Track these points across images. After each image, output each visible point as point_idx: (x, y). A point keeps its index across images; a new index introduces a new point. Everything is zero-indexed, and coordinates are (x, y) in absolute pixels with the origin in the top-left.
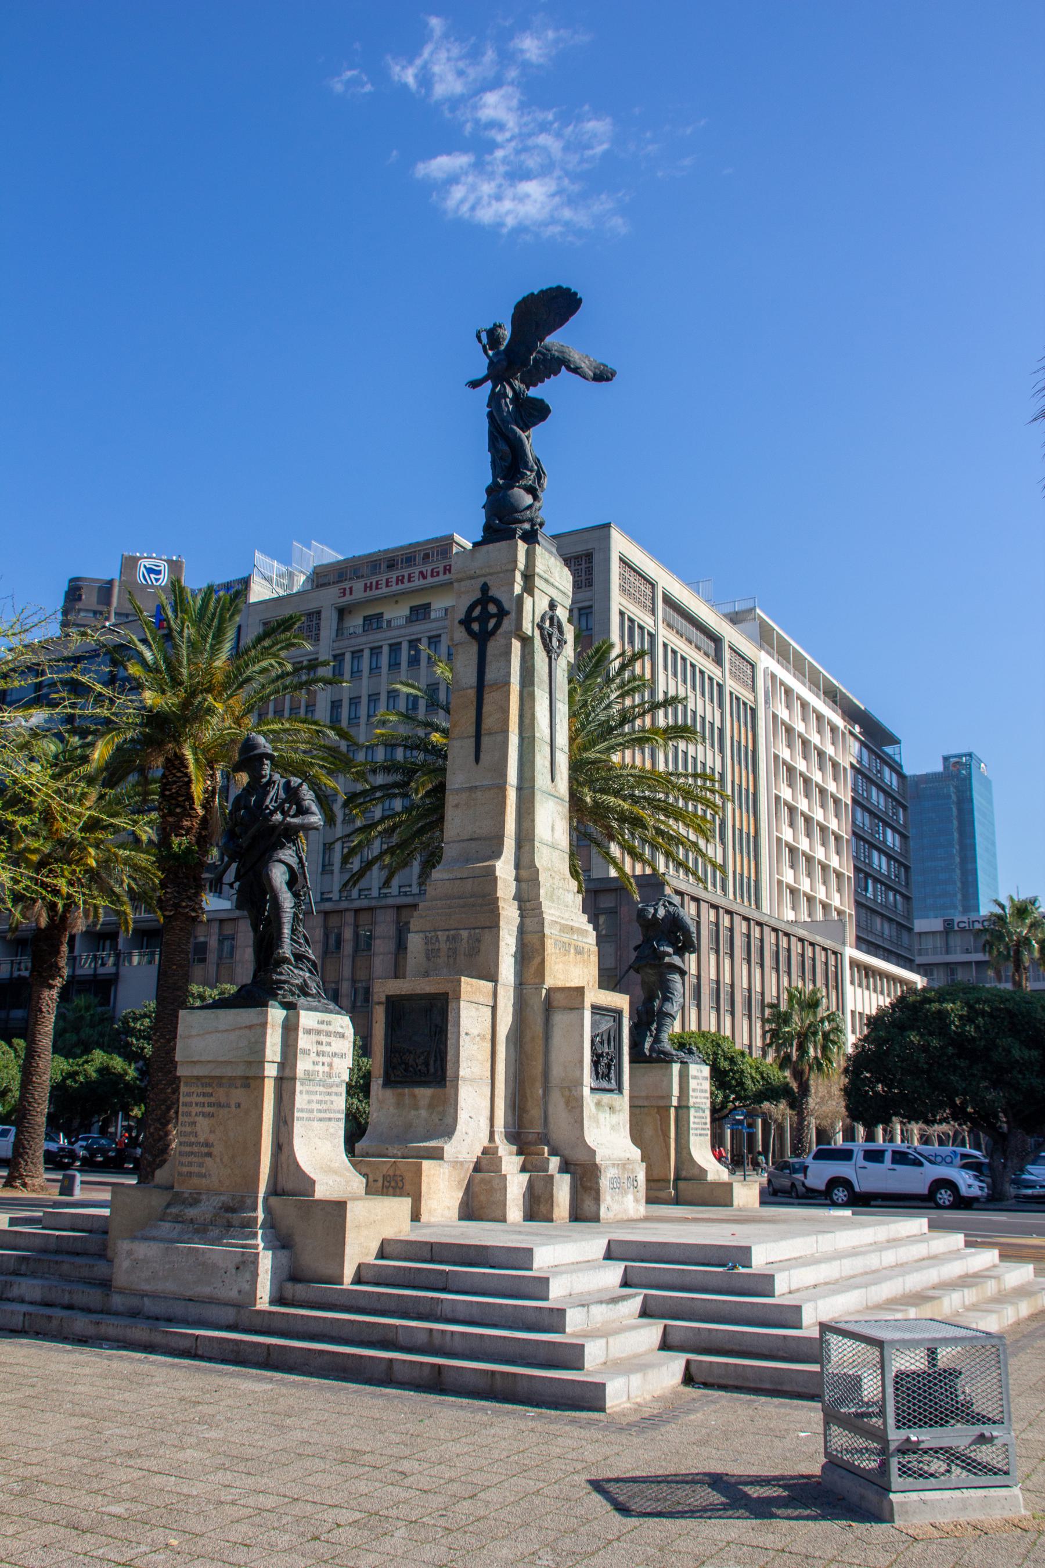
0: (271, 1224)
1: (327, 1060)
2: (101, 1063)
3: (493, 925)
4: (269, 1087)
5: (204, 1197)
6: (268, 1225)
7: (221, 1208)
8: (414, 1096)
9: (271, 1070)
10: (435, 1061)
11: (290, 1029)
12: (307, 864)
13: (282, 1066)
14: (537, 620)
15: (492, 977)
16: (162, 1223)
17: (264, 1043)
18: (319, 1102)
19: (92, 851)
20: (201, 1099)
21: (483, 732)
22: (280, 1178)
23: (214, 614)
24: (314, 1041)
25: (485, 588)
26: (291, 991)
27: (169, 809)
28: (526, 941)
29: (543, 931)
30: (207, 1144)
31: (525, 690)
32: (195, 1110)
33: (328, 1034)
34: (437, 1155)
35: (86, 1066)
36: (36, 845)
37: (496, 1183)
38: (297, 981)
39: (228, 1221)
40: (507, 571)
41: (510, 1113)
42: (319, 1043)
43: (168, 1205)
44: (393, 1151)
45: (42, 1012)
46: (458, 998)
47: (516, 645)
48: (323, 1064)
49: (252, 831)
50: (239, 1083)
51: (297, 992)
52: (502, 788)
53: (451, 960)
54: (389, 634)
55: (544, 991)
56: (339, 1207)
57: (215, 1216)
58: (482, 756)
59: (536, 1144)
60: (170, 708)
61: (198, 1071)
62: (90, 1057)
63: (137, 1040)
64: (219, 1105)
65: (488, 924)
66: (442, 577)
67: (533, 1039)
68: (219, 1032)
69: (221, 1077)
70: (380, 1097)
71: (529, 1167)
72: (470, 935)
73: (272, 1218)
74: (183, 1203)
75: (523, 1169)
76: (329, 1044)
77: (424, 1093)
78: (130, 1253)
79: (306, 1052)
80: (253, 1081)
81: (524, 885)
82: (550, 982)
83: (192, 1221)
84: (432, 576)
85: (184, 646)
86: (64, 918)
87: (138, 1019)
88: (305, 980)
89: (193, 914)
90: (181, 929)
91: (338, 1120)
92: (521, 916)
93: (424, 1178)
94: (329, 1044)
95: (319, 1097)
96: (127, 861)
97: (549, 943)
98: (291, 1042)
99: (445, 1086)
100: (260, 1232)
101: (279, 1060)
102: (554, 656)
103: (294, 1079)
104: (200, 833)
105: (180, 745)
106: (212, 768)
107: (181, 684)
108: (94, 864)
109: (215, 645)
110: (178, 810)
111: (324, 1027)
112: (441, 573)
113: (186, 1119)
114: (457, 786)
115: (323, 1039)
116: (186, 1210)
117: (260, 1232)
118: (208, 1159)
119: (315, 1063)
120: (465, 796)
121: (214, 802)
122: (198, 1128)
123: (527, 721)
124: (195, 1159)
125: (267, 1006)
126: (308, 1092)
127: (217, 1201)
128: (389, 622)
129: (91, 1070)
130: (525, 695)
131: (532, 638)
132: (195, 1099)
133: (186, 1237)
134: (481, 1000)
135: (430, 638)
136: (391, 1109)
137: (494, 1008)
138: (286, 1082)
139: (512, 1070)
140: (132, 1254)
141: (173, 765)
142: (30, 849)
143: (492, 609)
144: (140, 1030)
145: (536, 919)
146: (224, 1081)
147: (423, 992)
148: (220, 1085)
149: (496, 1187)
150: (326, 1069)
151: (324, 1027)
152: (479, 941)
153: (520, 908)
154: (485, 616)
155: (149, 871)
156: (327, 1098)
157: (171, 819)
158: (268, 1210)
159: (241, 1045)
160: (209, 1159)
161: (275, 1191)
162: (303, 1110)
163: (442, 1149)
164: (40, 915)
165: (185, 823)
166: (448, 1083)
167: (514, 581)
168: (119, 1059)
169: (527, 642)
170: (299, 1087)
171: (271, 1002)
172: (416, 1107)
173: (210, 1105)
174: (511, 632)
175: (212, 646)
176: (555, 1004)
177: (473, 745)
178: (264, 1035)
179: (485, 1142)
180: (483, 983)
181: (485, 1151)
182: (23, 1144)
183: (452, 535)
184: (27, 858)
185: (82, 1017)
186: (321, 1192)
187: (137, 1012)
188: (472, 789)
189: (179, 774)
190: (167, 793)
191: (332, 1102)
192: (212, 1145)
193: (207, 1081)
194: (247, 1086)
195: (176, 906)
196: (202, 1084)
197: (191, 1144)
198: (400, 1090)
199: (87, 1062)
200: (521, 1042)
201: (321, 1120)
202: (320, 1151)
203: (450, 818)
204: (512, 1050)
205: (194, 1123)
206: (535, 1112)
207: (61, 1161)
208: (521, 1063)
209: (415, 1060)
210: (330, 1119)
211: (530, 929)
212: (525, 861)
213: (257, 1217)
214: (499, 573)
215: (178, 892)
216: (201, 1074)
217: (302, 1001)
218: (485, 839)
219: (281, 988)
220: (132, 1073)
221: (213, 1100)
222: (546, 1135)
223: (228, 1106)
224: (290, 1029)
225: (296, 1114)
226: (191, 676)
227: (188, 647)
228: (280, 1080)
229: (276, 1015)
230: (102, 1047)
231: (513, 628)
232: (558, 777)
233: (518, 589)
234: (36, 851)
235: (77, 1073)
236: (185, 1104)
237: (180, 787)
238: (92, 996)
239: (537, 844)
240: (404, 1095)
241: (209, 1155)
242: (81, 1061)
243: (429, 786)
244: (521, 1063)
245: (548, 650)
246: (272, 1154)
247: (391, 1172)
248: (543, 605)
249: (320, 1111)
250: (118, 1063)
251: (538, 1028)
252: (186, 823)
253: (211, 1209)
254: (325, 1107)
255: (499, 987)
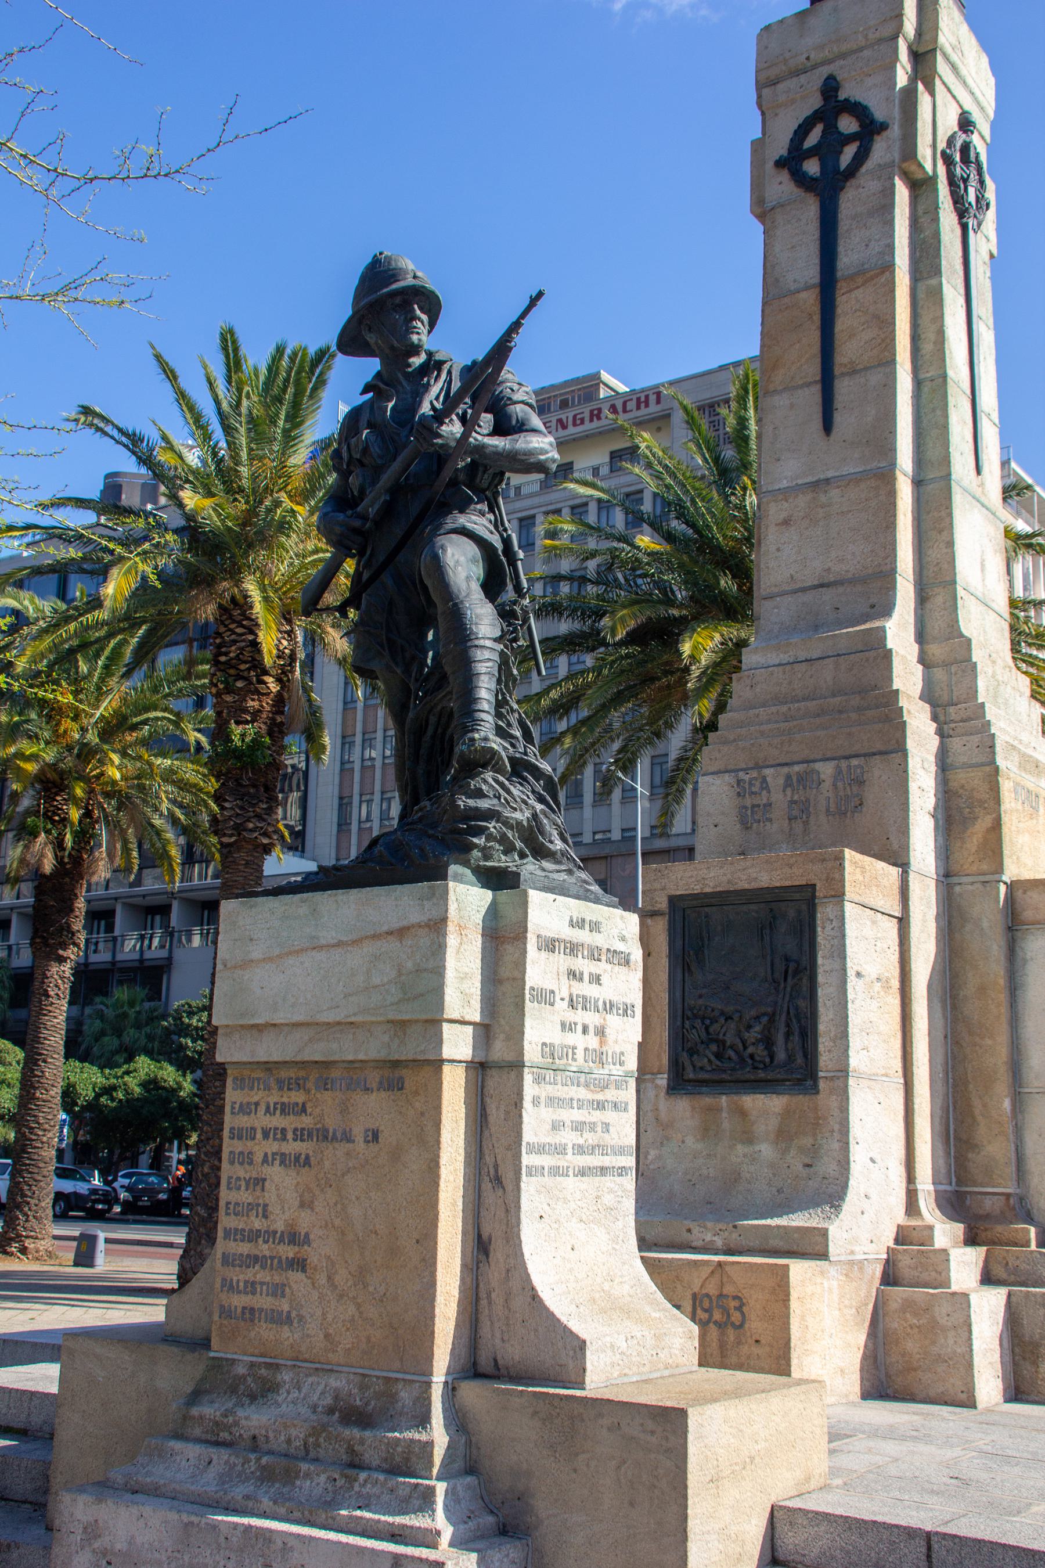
0: (468, 1462)
1: (592, 1019)
2: (147, 1074)
3: (895, 748)
4: (454, 1086)
5: (286, 1376)
6: (459, 1464)
7: (331, 1411)
8: (743, 1113)
9: (458, 1044)
10: (788, 1035)
11: (503, 938)
12: (521, 555)
13: (484, 1032)
14: (941, 145)
15: (897, 855)
16: (177, 1445)
17: (439, 971)
18: (579, 1127)
19: (116, 758)
20: (277, 1121)
21: (837, 371)
22: (485, 1331)
23: (287, 380)
24: (563, 969)
25: (830, 88)
26: (503, 839)
27: (226, 682)
28: (953, 785)
29: (993, 762)
30: (293, 1238)
31: (921, 287)
32: (261, 1148)
33: (595, 954)
34: (813, 1247)
35: (126, 1078)
36: (35, 749)
37: (941, 1312)
38: (518, 815)
39: (351, 1451)
40: (880, 41)
41: (940, 1146)
42: (574, 975)
43: (195, 1396)
44: (702, 1234)
45: (48, 996)
46: (839, 896)
47: (902, 193)
48: (585, 1030)
49: (386, 479)
50: (374, 1077)
51: (519, 844)
52: (887, 477)
53: (798, 827)
54: (518, 505)
55: (1003, 888)
56: (669, 1423)
57: (316, 1431)
58: (838, 418)
59: (1003, 1218)
60: (223, 521)
61: (269, 1049)
62: (132, 1066)
63: (194, 1041)
64: (324, 1135)
65: (879, 746)
66: (588, 426)
67: (982, 989)
68: (319, 948)
69: (327, 1065)
70: (663, 1115)
71: (999, 1272)
72: (839, 771)
73: (469, 1443)
74: (233, 1390)
75: (988, 1279)
76: (596, 979)
77: (766, 1107)
78: (92, 1532)
79: (546, 997)
80: (409, 1074)
81: (939, 674)
82: (1012, 871)
83: (255, 1443)
84: (575, 425)
85: (243, 430)
86: (77, 860)
87: (194, 1013)
88: (535, 816)
89: (265, 841)
90: (247, 863)
91: (622, 1171)
92: (940, 732)
93: (794, 1304)
94: (596, 979)
95: (577, 1115)
96: (169, 776)
97: (1006, 787)
98: (505, 972)
99: (815, 1090)
100: (441, 1488)
101: (477, 1017)
102: (971, 223)
103: (517, 1065)
104: (273, 719)
105: (238, 583)
106: (289, 622)
107: (241, 490)
108: (118, 776)
109: (290, 430)
110: (240, 684)
111: (582, 936)
112: (587, 419)
113: (241, 1172)
114: (785, 484)
115: (583, 965)
116: (241, 1413)
117: (441, 1488)
118: (296, 1277)
119: (567, 1027)
120: (802, 501)
121: (293, 672)
122: (270, 1196)
123: (927, 348)
124: (262, 1275)
125: (444, 877)
126: (553, 1102)
127: (321, 1390)
128: (518, 489)
129: (133, 1083)
130: (921, 295)
131: (932, 180)
132: (261, 1120)
133: (238, 1492)
134: (880, 903)
135: (573, 508)
136: (690, 1141)
137: (903, 922)
138: (496, 1075)
139: (940, 1059)
140: (98, 1536)
141: (231, 617)
142: (23, 754)
143: (848, 125)
144: (197, 1028)
145: (976, 739)
146: (335, 1073)
147: (754, 885)
148: (325, 1085)
149: (943, 1321)
150: (593, 1041)
151: (582, 936)
152: (861, 783)
153: (935, 718)
154: (833, 142)
155: (201, 790)
156: (597, 1116)
157: (229, 698)
158: (458, 1421)
159: (376, 980)
160: (300, 1276)
161: (475, 1366)
162: (540, 1149)
163: (824, 1233)
164: (43, 855)
165: (251, 703)
166: (822, 1084)
167: (896, 59)
168: (171, 1069)
169: (921, 187)
170: (530, 1088)
171: (453, 869)
172: (749, 1138)
173: (300, 1135)
174: (891, 165)
175: (286, 433)
176: (1028, 915)
177: (818, 398)
178: (439, 949)
179: (900, 1217)
180: (882, 866)
181: (902, 1237)
182: (22, 1190)
183: (599, 373)
184: (19, 767)
185: (125, 1015)
186: (604, 1374)
187: (194, 1004)
188: (816, 486)
189: (239, 630)
190: (223, 659)
191: (606, 1127)
192: (307, 1240)
193: (292, 1073)
194: (395, 1085)
195: (239, 829)
196: (280, 1084)
197: (253, 1236)
198: (708, 1100)
199: (128, 1073)
200: (954, 997)
201: (582, 1172)
202: (583, 1254)
203: (773, 548)
204: (939, 1014)
205: (259, 1182)
206: (995, 1149)
207: (93, 1207)
208: (957, 1043)
209: (739, 1034)
210: (603, 1171)
211: (963, 759)
212: (936, 625)
213: (430, 1444)
214: (861, 49)
215: (242, 808)
216: (276, 1057)
217: (530, 868)
218: (852, 581)
219: (480, 831)
220: (188, 1087)
221: (306, 1121)
222: (1021, 1199)
223: (347, 1138)
224: (503, 938)
225: (527, 1160)
226: (254, 478)
227: (249, 430)
228: (480, 1069)
229: (467, 900)
230: (150, 1053)
231: (897, 156)
232: (985, 469)
233: (902, 79)
234: (34, 758)
235: (114, 1088)
236: (238, 1134)
237: (242, 649)
238: (138, 989)
239: (960, 592)
240: (719, 1110)
241: (299, 1264)
242: (120, 1072)
243: (632, 624)
244: (957, 1043)
245: (962, 211)
246: (464, 1266)
247: (712, 1289)
248: (949, 122)
249: (580, 1150)
250: (169, 1074)
251: (996, 968)
252: (252, 704)
253: (304, 1410)
254: (590, 1138)
255: (912, 877)
